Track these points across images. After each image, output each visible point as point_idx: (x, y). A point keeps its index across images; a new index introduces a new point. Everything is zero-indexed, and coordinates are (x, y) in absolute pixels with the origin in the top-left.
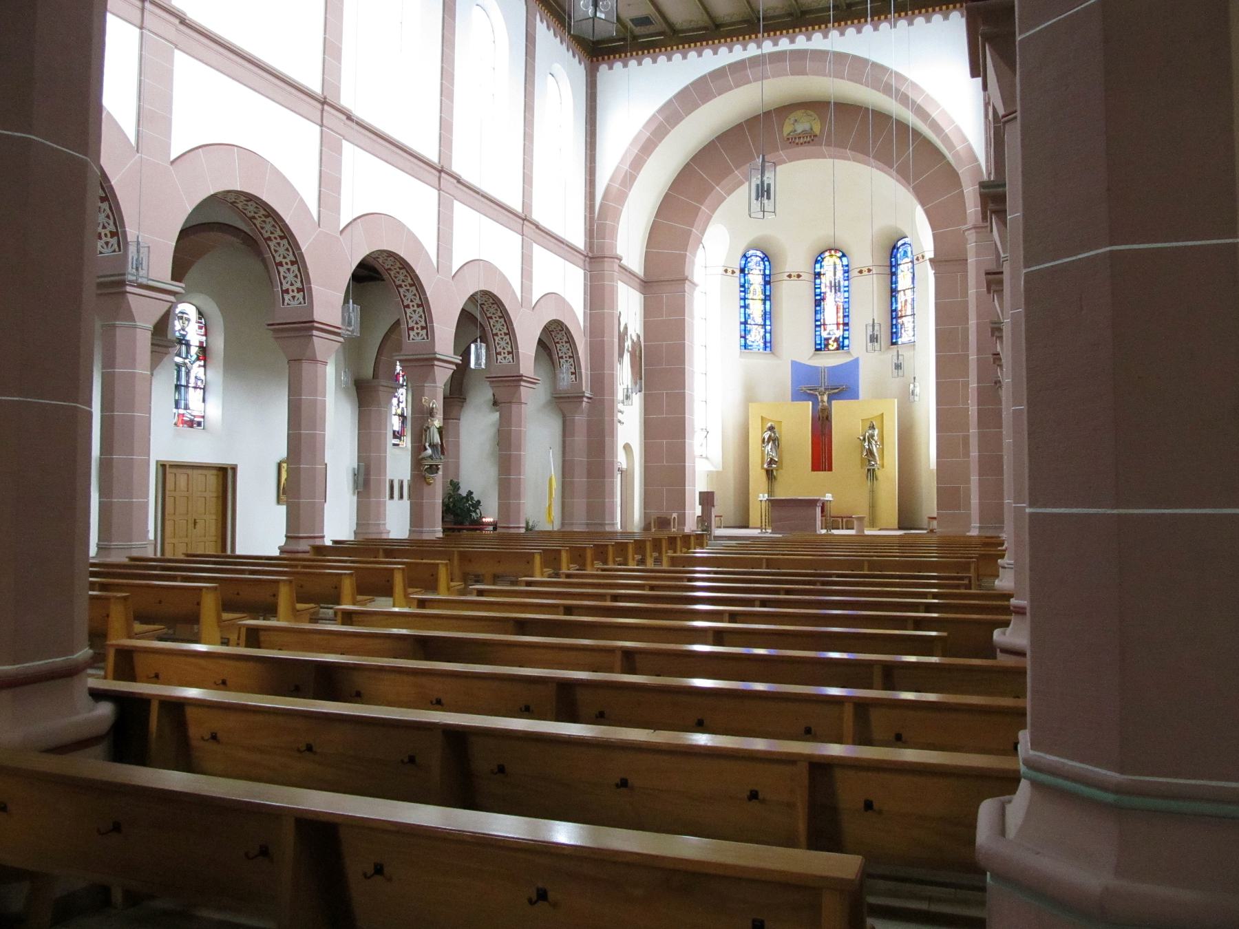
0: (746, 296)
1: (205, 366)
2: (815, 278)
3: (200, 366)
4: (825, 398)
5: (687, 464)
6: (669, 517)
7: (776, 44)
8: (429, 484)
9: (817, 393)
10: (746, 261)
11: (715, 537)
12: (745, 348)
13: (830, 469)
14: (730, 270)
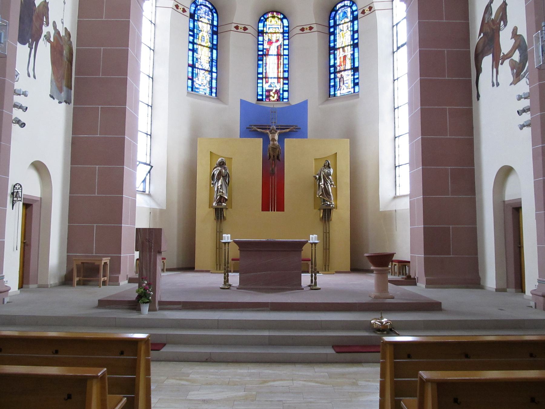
0: (195, 41)
2: (258, 36)
4: (276, 137)
5: (270, 302)
9: (268, 131)
10: (196, 7)
11: (161, 303)
12: (192, 90)
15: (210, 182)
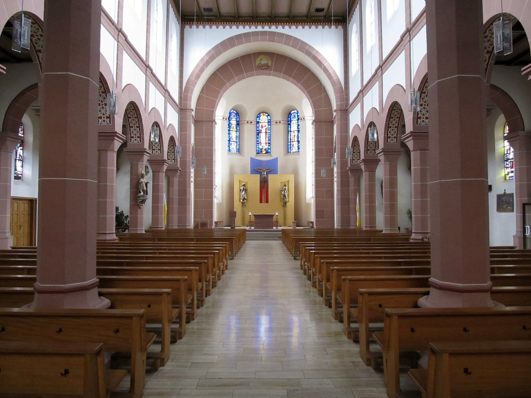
1: (22, 149)
3: (21, 149)
4: (265, 173)
7: (256, 28)
8: (140, 208)
9: (262, 171)
12: (229, 151)
13: (268, 203)
14: (225, 118)
15: (240, 192)
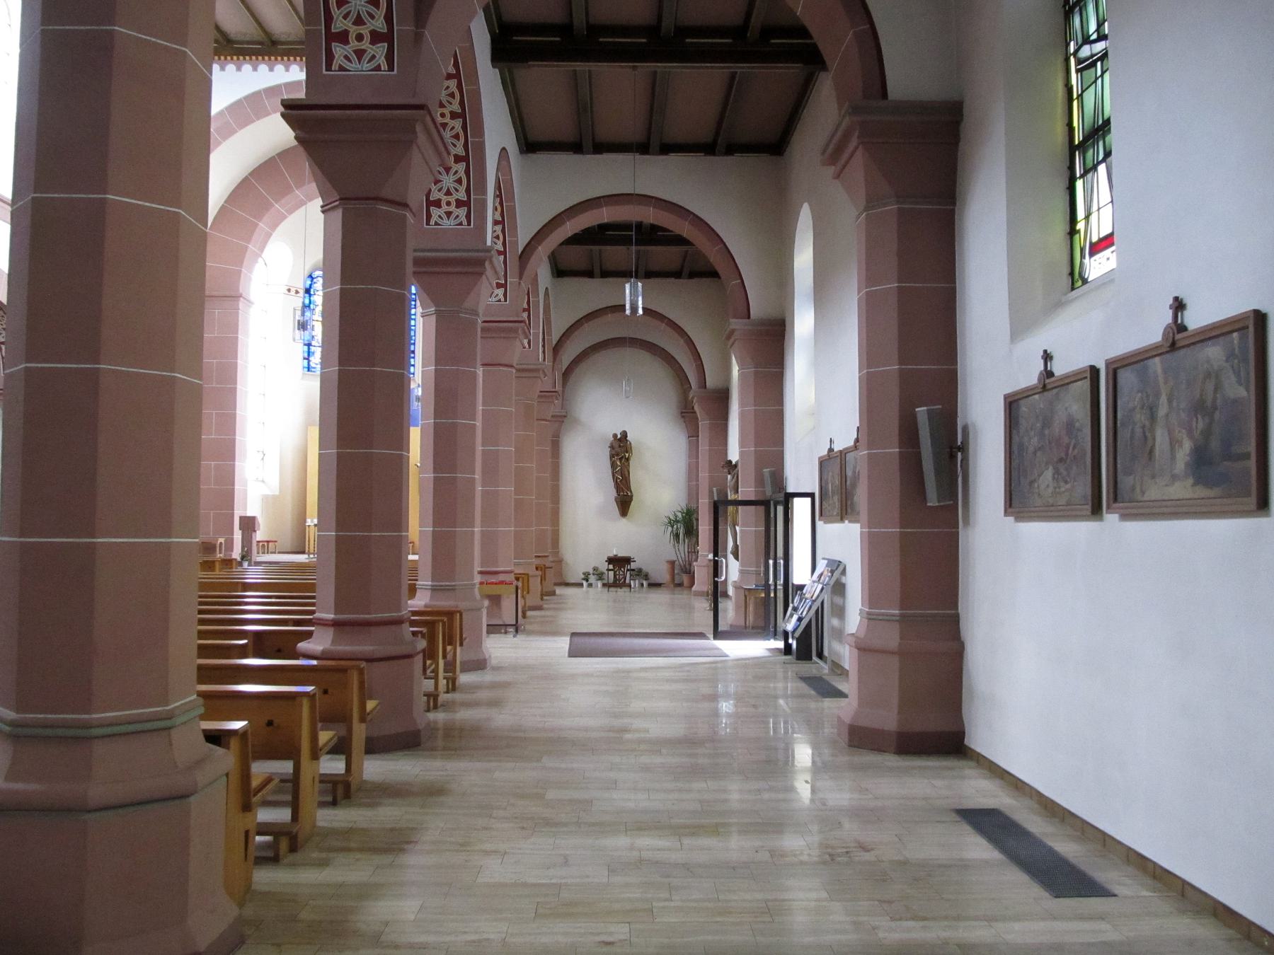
6: (213, 542)
10: (312, 281)
12: (309, 370)
14: (293, 290)
